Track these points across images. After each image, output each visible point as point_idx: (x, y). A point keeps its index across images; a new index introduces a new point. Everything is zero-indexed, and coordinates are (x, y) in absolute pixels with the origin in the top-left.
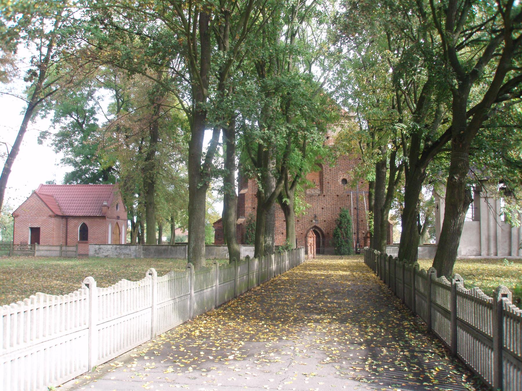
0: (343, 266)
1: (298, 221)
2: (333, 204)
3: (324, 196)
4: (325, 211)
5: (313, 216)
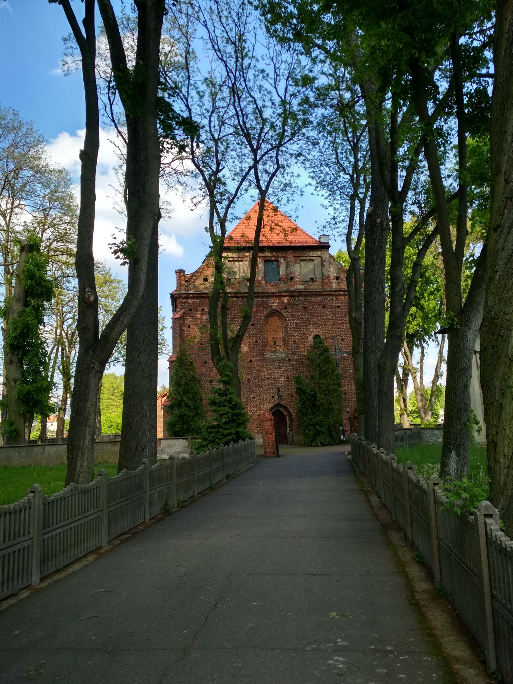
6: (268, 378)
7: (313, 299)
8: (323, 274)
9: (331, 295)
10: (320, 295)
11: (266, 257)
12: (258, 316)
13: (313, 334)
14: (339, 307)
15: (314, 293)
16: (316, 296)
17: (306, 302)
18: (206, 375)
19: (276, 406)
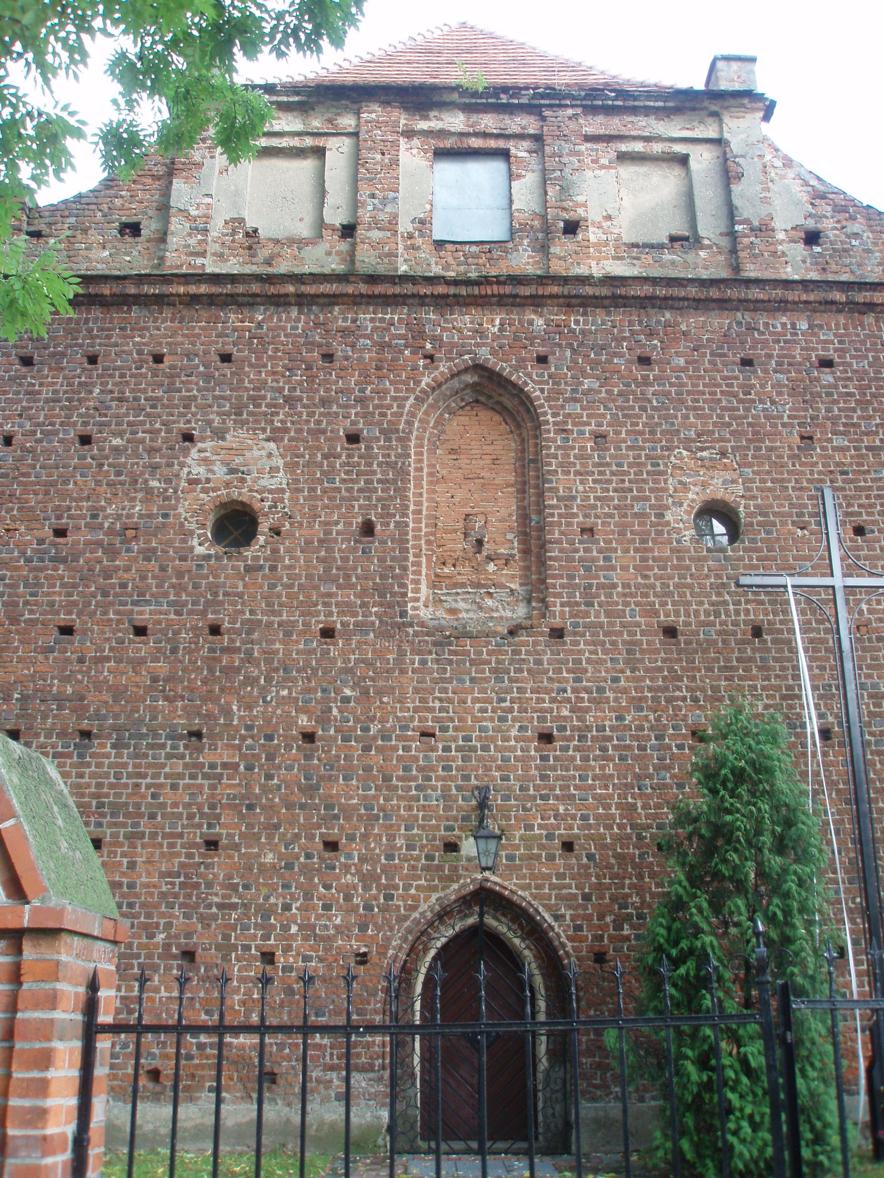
0: (647, 111)
1: (332, 846)
2: (638, 703)
3: (558, 633)
4: (566, 763)
5: (464, 803)
6: (426, 734)
7: (690, 322)
8: (731, 212)
9: (783, 306)
10: (723, 304)
11: (442, 134)
12: (381, 393)
13: (694, 497)
14: (826, 363)
15: (693, 291)
16: (699, 304)
17: (651, 335)
18: (61, 699)
19: (467, 901)
